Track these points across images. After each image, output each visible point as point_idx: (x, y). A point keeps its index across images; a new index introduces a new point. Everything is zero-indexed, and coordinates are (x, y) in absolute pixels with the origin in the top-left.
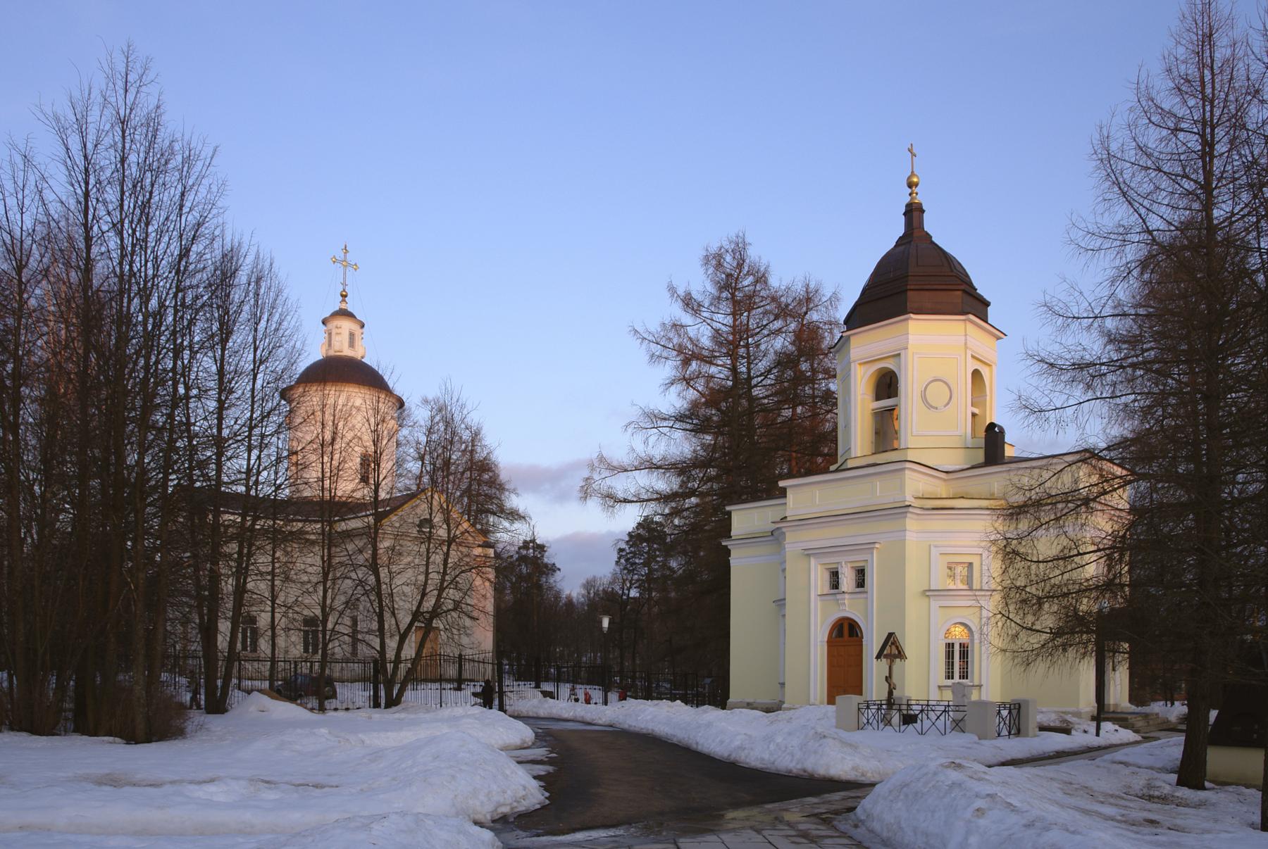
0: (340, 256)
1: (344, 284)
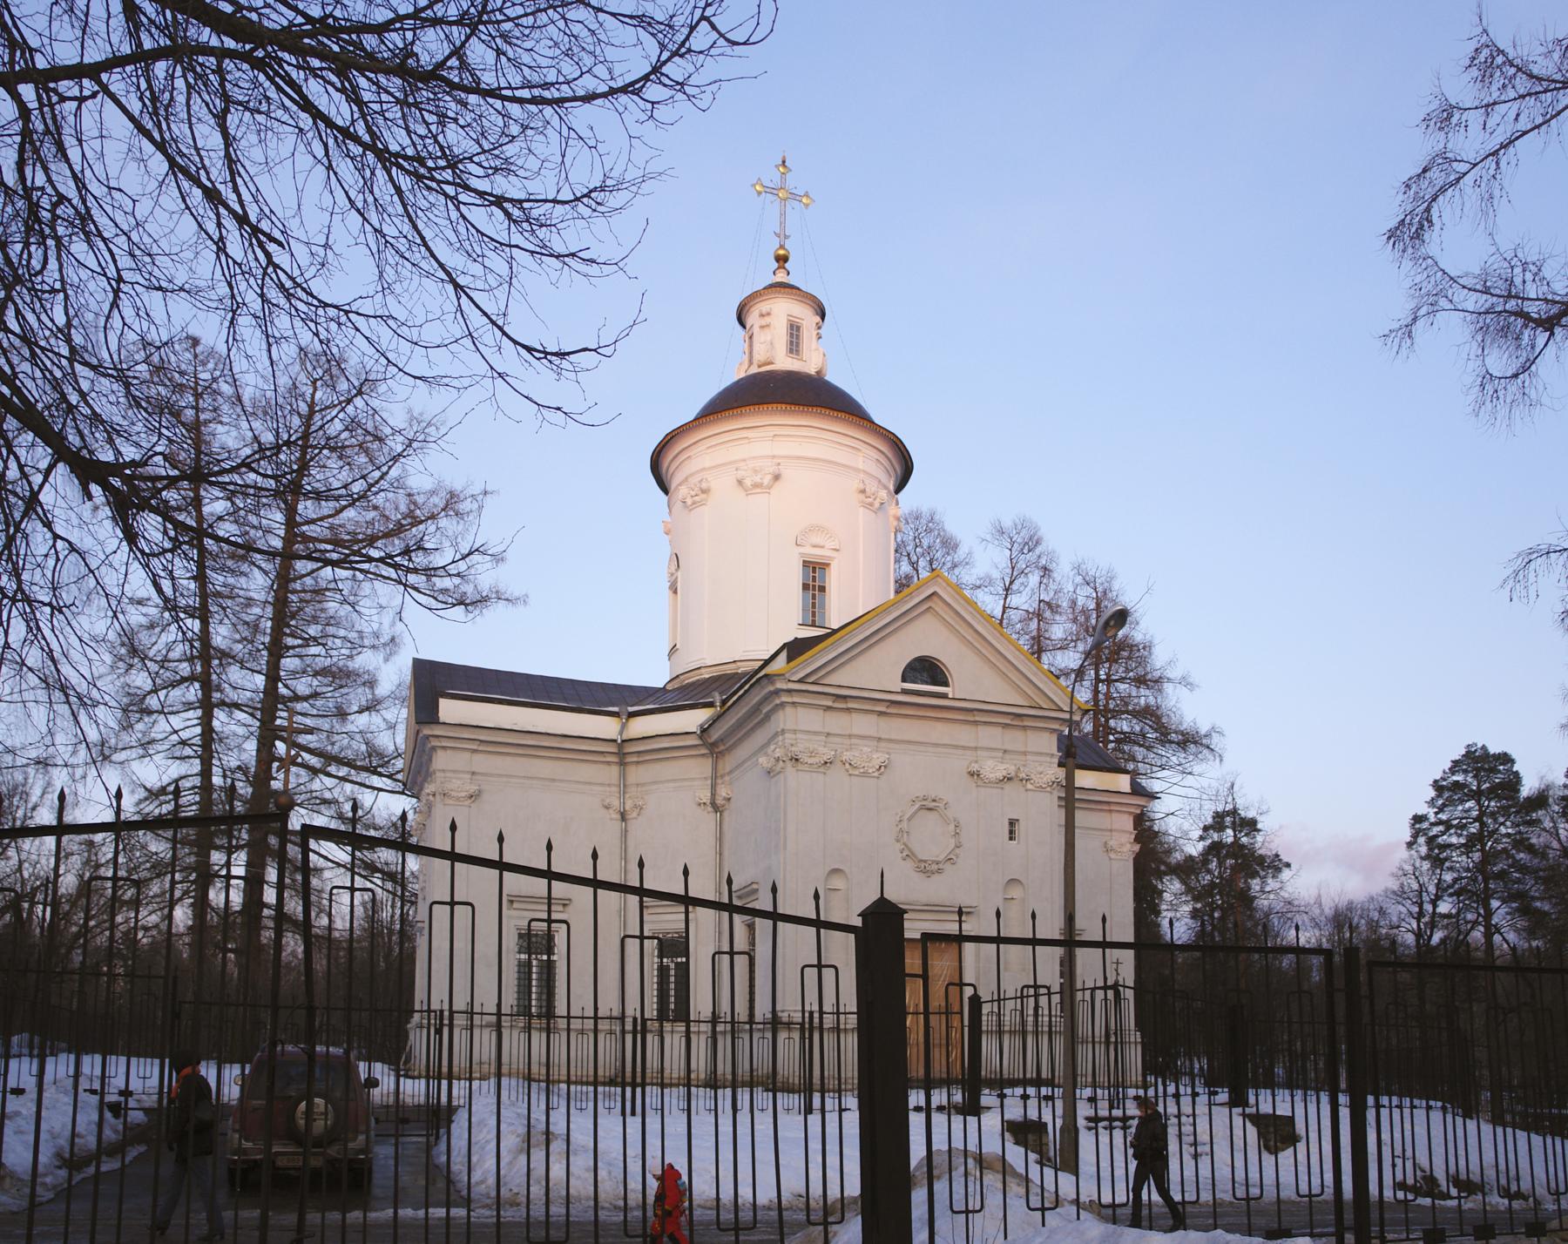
0: (772, 176)
1: (783, 236)
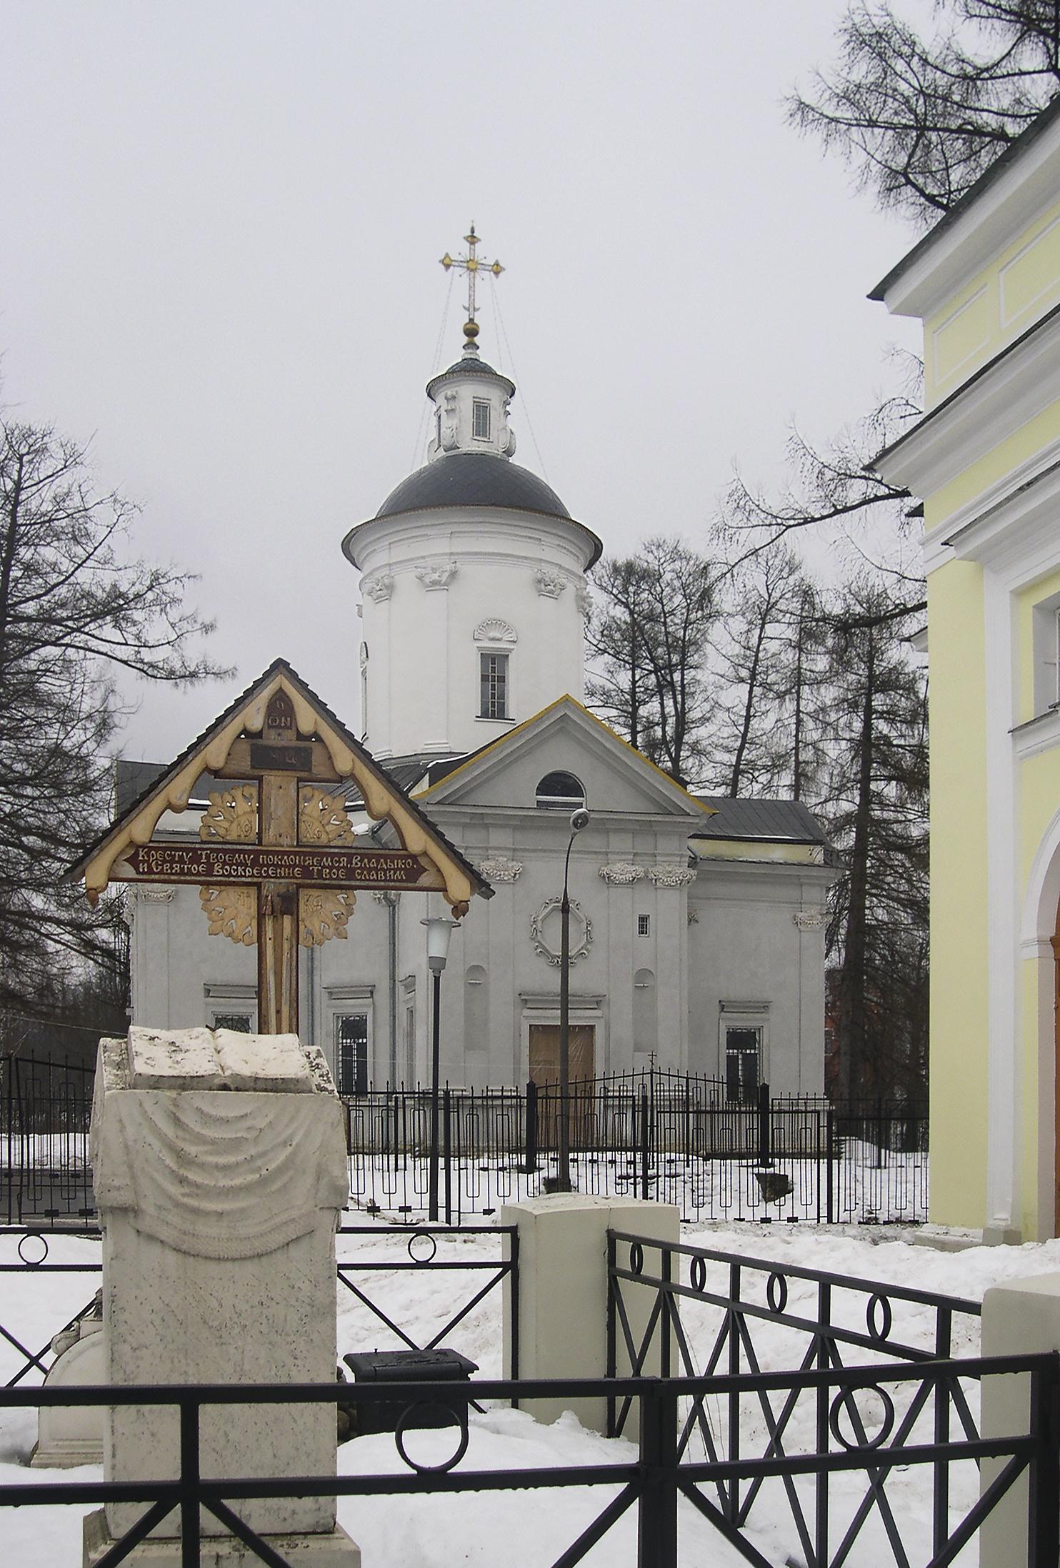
0: (460, 250)
1: (472, 308)
